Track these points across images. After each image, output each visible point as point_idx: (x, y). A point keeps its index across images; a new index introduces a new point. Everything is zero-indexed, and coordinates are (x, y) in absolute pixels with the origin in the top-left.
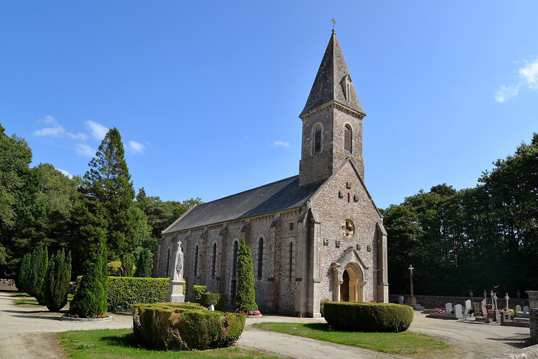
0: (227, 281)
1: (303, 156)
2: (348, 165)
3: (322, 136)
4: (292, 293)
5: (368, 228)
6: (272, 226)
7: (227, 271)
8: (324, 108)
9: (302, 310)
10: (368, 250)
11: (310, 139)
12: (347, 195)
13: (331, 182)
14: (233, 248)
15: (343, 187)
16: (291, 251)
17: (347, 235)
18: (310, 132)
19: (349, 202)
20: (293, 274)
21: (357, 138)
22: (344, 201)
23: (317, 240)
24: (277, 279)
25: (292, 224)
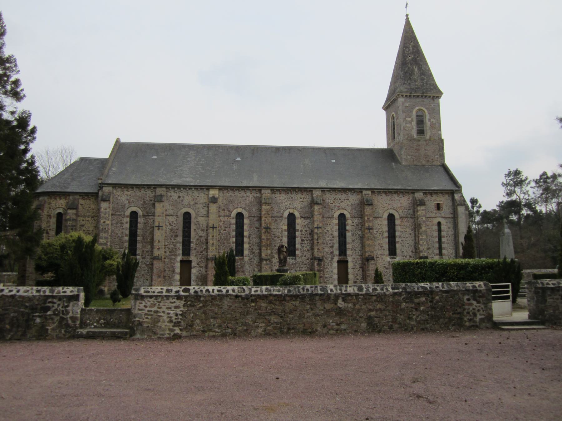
8: (430, 97)
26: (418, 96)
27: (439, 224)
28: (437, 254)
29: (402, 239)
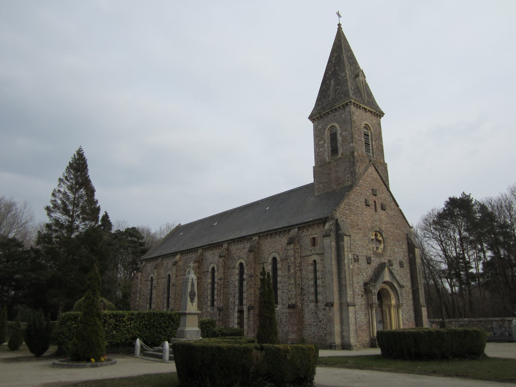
0: (231, 311)
1: (316, 162)
2: (371, 169)
3: (339, 138)
4: (320, 322)
5: (398, 241)
6: (289, 243)
7: (231, 299)
8: (339, 107)
9: (338, 341)
10: (401, 264)
11: (325, 142)
12: (373, 204)
13: (357, 189)
14: (237, 271)
15: (368, 194)
16: (315, 271)
17: (377, 248)
18: (324, 134)
19: (376, 211)
20: (320, 297)
21: (377, 139)
22: (371, 210)
23: (348, 256)
24: (299, 305)
25: (314, 238)
26: (328, 113)
27: (315, 261)
28: (312, 301)
29: (283, 284)
